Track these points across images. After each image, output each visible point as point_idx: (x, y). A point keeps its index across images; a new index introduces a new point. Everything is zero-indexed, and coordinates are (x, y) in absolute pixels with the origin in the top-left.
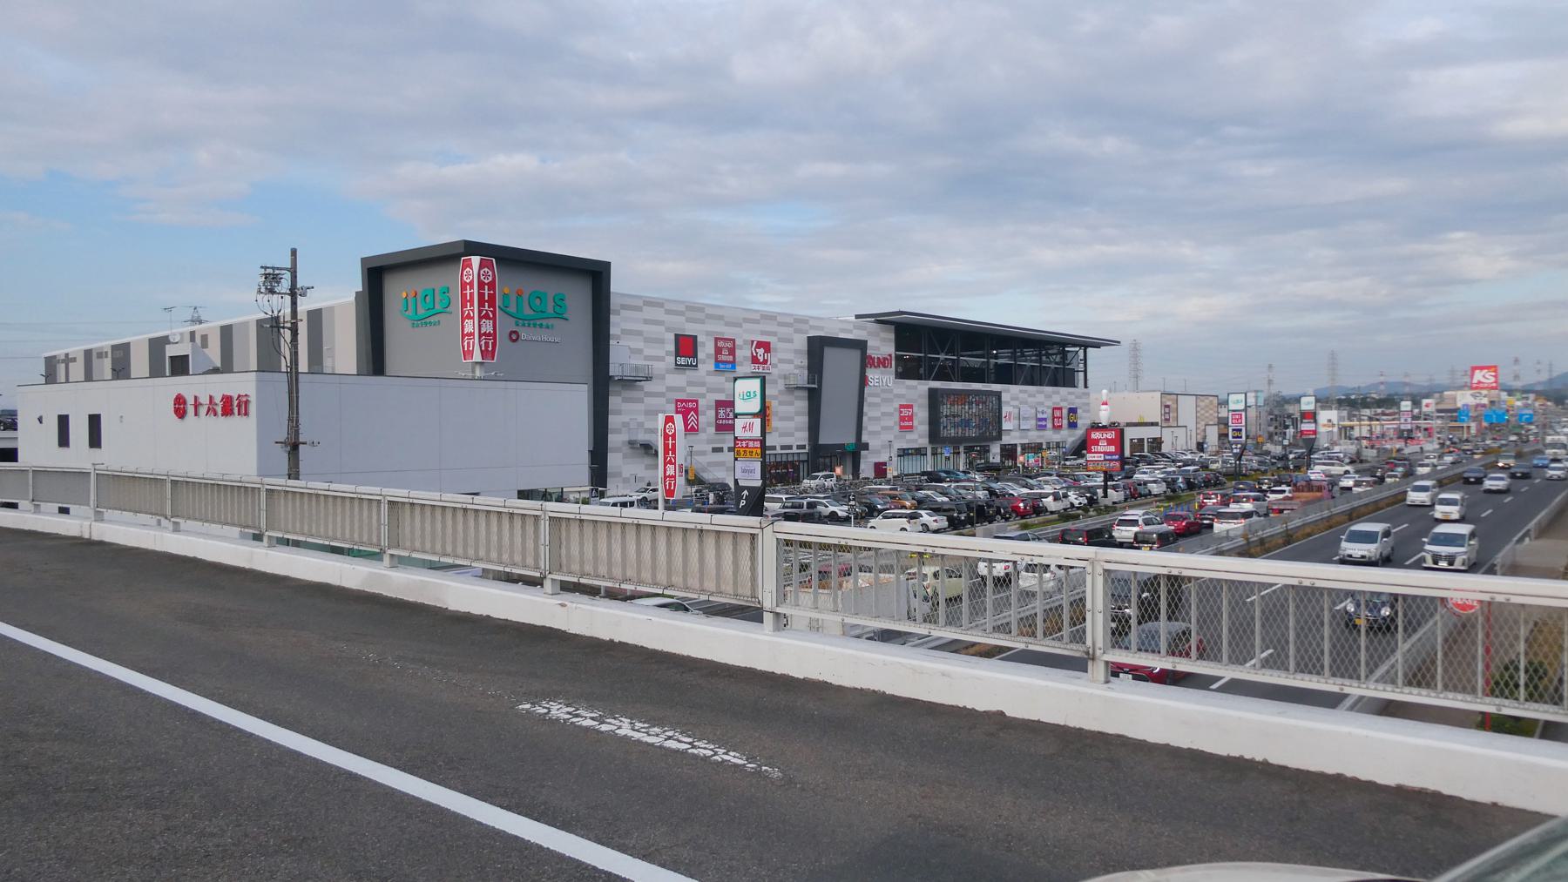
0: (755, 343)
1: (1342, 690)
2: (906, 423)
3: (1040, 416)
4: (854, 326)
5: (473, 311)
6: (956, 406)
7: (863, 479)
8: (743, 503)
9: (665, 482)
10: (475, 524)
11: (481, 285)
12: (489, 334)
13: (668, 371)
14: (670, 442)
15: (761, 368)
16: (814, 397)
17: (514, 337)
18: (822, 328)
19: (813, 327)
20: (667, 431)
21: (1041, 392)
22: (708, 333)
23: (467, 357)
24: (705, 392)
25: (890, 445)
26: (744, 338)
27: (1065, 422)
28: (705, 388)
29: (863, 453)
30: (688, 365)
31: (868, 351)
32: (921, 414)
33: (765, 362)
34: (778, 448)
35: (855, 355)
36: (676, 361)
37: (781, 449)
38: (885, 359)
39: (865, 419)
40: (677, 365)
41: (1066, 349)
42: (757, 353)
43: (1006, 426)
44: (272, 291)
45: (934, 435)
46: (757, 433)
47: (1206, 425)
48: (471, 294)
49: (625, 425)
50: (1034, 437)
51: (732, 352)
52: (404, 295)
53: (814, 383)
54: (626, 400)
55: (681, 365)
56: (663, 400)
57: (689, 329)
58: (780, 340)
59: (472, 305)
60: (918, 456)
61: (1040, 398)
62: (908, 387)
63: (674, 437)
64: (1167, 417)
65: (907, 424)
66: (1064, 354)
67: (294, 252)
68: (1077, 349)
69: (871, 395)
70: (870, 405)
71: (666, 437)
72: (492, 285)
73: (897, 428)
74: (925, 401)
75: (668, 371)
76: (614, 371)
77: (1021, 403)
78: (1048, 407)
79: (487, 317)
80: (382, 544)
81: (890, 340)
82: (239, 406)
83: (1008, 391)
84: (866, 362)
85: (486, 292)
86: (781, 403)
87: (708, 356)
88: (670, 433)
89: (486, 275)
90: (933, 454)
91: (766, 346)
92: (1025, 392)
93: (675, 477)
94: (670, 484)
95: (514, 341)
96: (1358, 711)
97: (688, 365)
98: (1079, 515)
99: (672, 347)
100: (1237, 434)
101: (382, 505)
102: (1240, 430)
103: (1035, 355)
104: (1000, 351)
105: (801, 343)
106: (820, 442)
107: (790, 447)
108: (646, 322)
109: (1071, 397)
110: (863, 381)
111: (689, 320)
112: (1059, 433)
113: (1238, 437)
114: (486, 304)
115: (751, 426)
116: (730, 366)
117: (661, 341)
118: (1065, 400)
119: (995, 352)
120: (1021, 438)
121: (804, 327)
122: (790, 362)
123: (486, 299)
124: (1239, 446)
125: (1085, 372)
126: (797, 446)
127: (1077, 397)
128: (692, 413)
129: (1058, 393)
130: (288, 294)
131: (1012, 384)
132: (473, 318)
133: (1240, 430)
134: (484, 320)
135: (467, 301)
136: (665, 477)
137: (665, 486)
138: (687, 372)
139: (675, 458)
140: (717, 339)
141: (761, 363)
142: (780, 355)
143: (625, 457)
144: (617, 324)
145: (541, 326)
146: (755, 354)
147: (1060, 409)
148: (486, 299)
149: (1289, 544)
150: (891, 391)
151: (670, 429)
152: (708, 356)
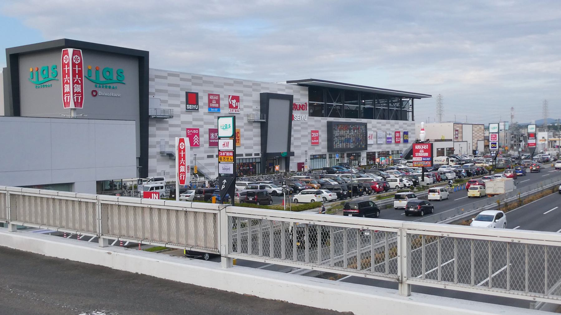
0: (231, 97)
2: (315, 141)
3: (388, 136)
5: (69, 79)
8: (223, 187)
9: (179, 176)
11: (74, 65)
12: (79, 93)
14: (182, 153)
15: (234, 110)
16: (264, 126)
19: (263, 88)
20: (180, 147)
22: (204, 91)
23: (66, 106)
25: (306, 154)
29: (291, 157)
32: (323, 136)
33: (237, 107)
34: (244, 155)
35: (287, 103)
36: (186, 107)
37: (246, 156)
38: (303, 105)
39: (292, 139)
40: (187, 109)
41: (402, 99)
42: (232, 102)
43: (369, 142)
46: (231, 147)
47: (478, 141)
48: (68, 70)
49: (158, 143)
50: (385, 148)
51: (218, 102)
53: (264, 119)
54: (158, 129)
55: (189, 109)
57: (194, 89)
58: (245, 95)
59: (69, 76)
61: (388, 126)
63: (184, 150)
66: (401, 102)
68: (408, 99)
69: (295, 125)
71: (180, 150)
72: (80, 65)
75: (182, 113)
78: (393, 131)
79: (77, 83)
83: (371, 123)
84: (293, 107)
85: (77, 69)
86: (245, 130)
87: (205, 104)
88: (182, 148)
89: (77, 59)
91: (237, 99)
93: (185, 173)
97: (193, 109)
99: (184, 99)
101: (7, 196)
103: (386, 103)
104: (366, 101)
106: (267, 152)
107: (251, 155)
108: (170, 85)
110: (291, 118)
114: (77, 76)
115: (228, 143)
116: (216, 110)
117: (178, 96)
119: (363, 101)
120: (378, 148)
122: (251, 107)
123: (77, 72)
128: (196, 136)
129: (398, 124)
132: (69, 84)
134: (76, 85)
136: (180, 173)
137: (180, 178)
139: (185, 162)
140: (209, 95)
142: (245, 104)
143: (158, 161)
144: (153, 86)
146: (231, 103)
147: (399, 132)
148: (77, 72)
149: (521, 205)
150: (306, 123)
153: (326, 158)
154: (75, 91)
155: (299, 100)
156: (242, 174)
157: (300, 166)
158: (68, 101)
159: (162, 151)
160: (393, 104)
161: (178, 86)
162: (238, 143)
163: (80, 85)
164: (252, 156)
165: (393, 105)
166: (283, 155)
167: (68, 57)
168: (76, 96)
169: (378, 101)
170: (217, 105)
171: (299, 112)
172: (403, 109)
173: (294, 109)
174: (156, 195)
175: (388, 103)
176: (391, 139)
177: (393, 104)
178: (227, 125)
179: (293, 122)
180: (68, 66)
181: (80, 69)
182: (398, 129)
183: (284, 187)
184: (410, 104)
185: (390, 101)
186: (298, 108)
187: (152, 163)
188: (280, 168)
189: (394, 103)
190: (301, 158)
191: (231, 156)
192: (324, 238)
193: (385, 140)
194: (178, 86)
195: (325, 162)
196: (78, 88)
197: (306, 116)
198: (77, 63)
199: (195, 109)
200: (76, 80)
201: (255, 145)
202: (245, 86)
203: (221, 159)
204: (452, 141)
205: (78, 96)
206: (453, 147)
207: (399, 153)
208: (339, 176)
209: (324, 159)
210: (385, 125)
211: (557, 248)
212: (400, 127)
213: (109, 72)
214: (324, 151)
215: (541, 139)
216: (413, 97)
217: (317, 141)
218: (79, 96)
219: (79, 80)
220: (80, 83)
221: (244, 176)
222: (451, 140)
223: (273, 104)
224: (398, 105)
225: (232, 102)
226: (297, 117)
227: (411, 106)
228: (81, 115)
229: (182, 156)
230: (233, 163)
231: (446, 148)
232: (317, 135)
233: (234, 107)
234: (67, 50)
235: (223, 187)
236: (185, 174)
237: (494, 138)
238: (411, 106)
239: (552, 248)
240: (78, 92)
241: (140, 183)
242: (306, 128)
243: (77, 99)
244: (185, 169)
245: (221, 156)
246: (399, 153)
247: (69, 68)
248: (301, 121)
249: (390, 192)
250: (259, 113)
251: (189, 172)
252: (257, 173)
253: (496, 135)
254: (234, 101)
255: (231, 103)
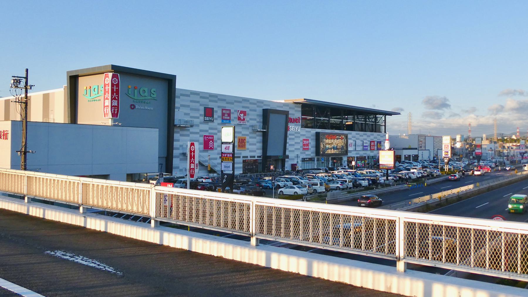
0: (240, 111)
1: (435, 265)
2: (305, 147)
3: (365, 145)
4: (283, 105)
5: (109, 96)
6: (328, 140)
7: (286, 171)
8: (224, 181)
9: (190, 171)
10: (5, 176)
11: (113, 85)
12: (116, 106)
13: (201, 123)
14: (193, 154)
15: (242, 122)
16: (265, 136)
17: (133, 107)
18: (269, 105)
19: (265, 105)
20: (191, 149)
21: (366, 134)
22: (219, 107)
23: (106, 116)
24: (217, 132)
25: (297, 156)
26: (234, 108)
27: (376, 147)
28: (217, 131)
29: (286, 160)
30: (209, 121)
31: (289, 116)
32: (312, 143)
33: (244, 119)
34: (249, 157)
35: (284, 117)
36: (204, 119)
37: (250, 158)
38: (296, 119)
39: (287, 145)
40: (205, 120)
41: (377, 116)
42: (240, 116)
43: (350, 149)
44: (17, 87)
45: (317, 152)
46: (231, 150)
47: (438, 149)
48: (108, 89)
49: (181, 146)
50: (362, 153)
51: (229, 115)
52: (85, 88)
53: (265, 129)
54: (181, 135)
55: (206, 120)
56: (198, 136)
57: (211, 105)
58: (251, 110)
59: (108, 94)
60: (311, 161)
61: (365, 137)
62: (307, 131)
63: (194, 152)
64: (421, 146)
65: (306, 147)
66: (376, 118)
67: (27, 70)
68: (382, 116)
69: (290, 135)
70: (290, 139)
71: (191, 152)
72: (117, 85)
73: (301, 149)
74: (314, 138)
75: (201, 123)
76: (176, 122)
77: (357, 139)
78: (368, 141)
79: (115, 99)
80: (251, 231)
81: (299, 111)
82: (3, 135)
83: (351, 134)
84: (288, 120)
85: (115, 88)
86: (250, 138)
87: (219, 117)
88: (193, 150)
89: (115, 81)
90: (317, 161)
91: (244, 113)
92: (359, 134)
93: (194, 169)
94: (192, 172)
95: (132, 109)
96: (453, 276)
97: (209, 121)
98: (374, 188)
99: (202, 112)
100: (446, 154)
101: (80, 185)
102: (448, 152)
103: (364, 118)
104: (348, 116)
105: (260, 111)
106: (267, 155)
107: (254, 157)
108: (192, 101)
109: (379, 137)
110: (287, 129)
111: (210, 101)
112: (373, 152)
113: (447, 155)
114: (115, 93)
115: (229, 147)
116: (227, 121)
117: (198, 110)
118: (376, 138)
119: (346, 117)
120: (356, 154)
121: (262, 105)
122: (255, 120)
123: (115, 91)
124: (447, 159)
125: (385, 126)
126: (257, 156)
127: (381, 137)
128: (211, 141)
129: (373, 135)
130: (24, 88)
131: (352, 131)
132: (109, 99)
133: (448, 152)
134: (114, 100)
135: (106, 92)
136: (190, 169)
137: (190, 173)
138: (209, 123)
139: (194, 161)
140: (223, 110)
141: (242, 120)
142: (250, 117)
143: (181, 160)
144: (178, 102)
145: (144, 102)
146: (239, 116)
147: (374, 142)
148: (115, 91)
149: (459, 201)
150: (299, 133)
151: (193, 148)
152: (219, 117)
153: (314, 161)
154: (113, 105)
155: (293, 114)
156: (247, 171)
157: (294, 166)
158: (107, 112)
159: (184, 152)
160: (370, 119)
161: (198, 102)
162: (245, 147)
163: (117, 101)
164: (255, 158)
165: (369, 120)
166: (279, 158)
167: (108, 79)
168: (113, 109)
169: (358, 117)
170: (228, 118)
171: (293, 124)
172: (377, 124)
173: (290, 122)
174: (171, 186)
175: (365, 119)
176: (367, 147)
177: (370, 119)
178: (228, 133)
179: (288, 132)
180: (108, 86)
181: (117, 88)
182: (373, 139)
183: (273, 182)
184: (383, 120)
185: (367, 117)
186: (293, 121)
187: (176, 162)
188: (275, 167)
189: (371, 118)
190: (294, 160)
191: (231, 157)
192: (286, 222)
193: (362, 147)
194: (198, 102)
195: (314, 164)
196: (115, 103)
197: (299, 127)
198: (115, 83)
199: (211, 121)
200: (114, 97)
201: (258, 149)
202: (251, 103)
203: (223, 159)
204: (417, 149)
205: (115, 108)
206: (418, 154)
207: (373, 158)
208: (316, 175)
209: (313, 162)
210: (362, 136)
211: (510, 234)
212: (375, 138)
213: (145, 90)
214: (313, 155)
215: (489, 149)
216: (386, 114)
217: (308, 147)
218: (116, 109)
219: (116, 97)
220: (117, 99)
221: (248, 174)
222: (416, 149)
223: (272, 117)
224: (373, 120)
225: (240, 116)
226: (292, 128)
227: (384, 121)
228: (117, 123)
229: (192, 156)
230: (232, 162)
231: (412, 155)
232: (308, 143)
233: (242, 119)
234: (108, 74)
235: (224, 181)
236: (194, 170)
237: (447, 147)
238: (384, 121)
239: (513, 235)
240: (115, 105)
241: (161, 176)
242: (299, 137)
243: (114, 111)
244: (194, 166)
245: (223, 157)
246: (374, 158)
247: (109, 87)
248: (295, 131)
249: (360, 188)
250: (262, 124)
251: (197, 168)
252: (259, 171)
253: (448, 145)
254: (242, 115)
255: (239, 116)
